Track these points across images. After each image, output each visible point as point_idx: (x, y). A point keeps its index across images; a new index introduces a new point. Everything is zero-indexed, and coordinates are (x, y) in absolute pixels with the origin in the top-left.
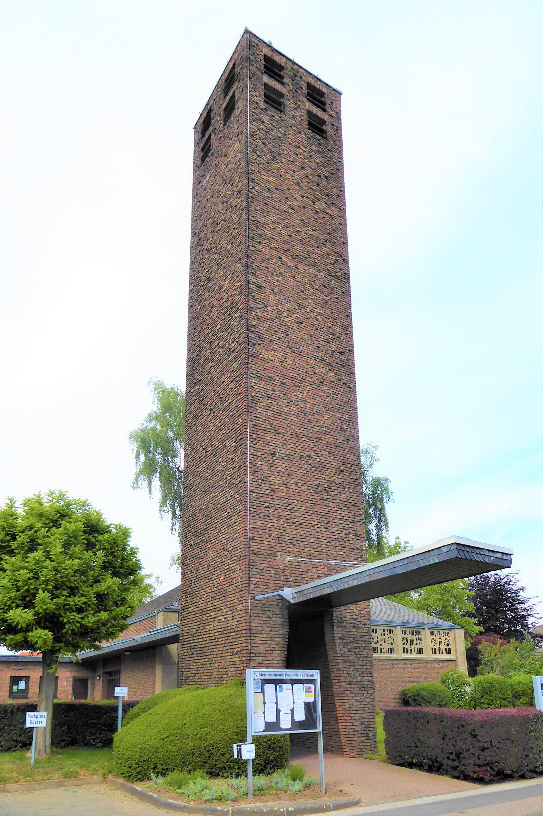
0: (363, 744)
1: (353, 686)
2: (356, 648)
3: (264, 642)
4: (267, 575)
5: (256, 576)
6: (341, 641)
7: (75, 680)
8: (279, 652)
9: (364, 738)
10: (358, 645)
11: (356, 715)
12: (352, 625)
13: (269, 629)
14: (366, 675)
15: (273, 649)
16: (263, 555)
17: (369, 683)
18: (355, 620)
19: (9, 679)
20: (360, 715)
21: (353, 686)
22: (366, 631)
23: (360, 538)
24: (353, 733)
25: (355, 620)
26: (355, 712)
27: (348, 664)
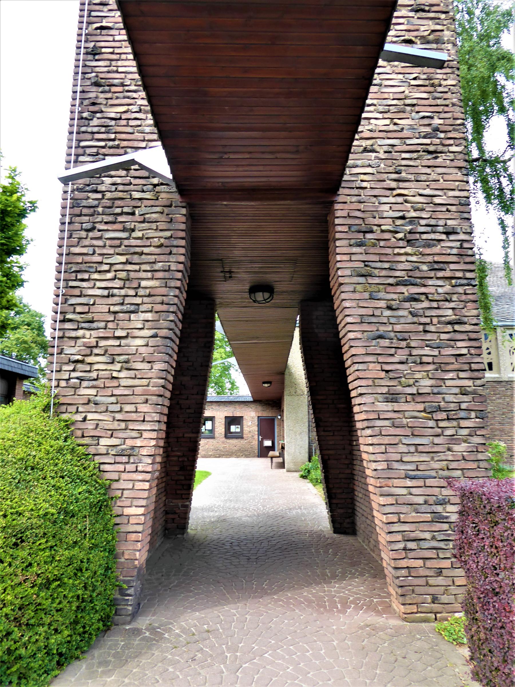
0: (440, 580)
1: (404, 407)
2: (413, 299)
3: (106, 292)
4: (129, 130)
5: (97, 136)
6: (362, 280)
7: (260, 420)
8: (149, 316)
9: (447, 564)
10: (423, 290)
11: (414, 491)
12: (400, 235)
13: (123, 259)
14: (451, 375)
15: (132, 308)
16: (123, 85)
17: (465, 398)
18: (412, 221)
19: (224, 420)
20: (429, 491)
21: (404, 407)
22: (455, 251)
23: (432, 15)
24: (401, 545)
25: (411, 223)
26: (409, 483)
27: (386, 343)
